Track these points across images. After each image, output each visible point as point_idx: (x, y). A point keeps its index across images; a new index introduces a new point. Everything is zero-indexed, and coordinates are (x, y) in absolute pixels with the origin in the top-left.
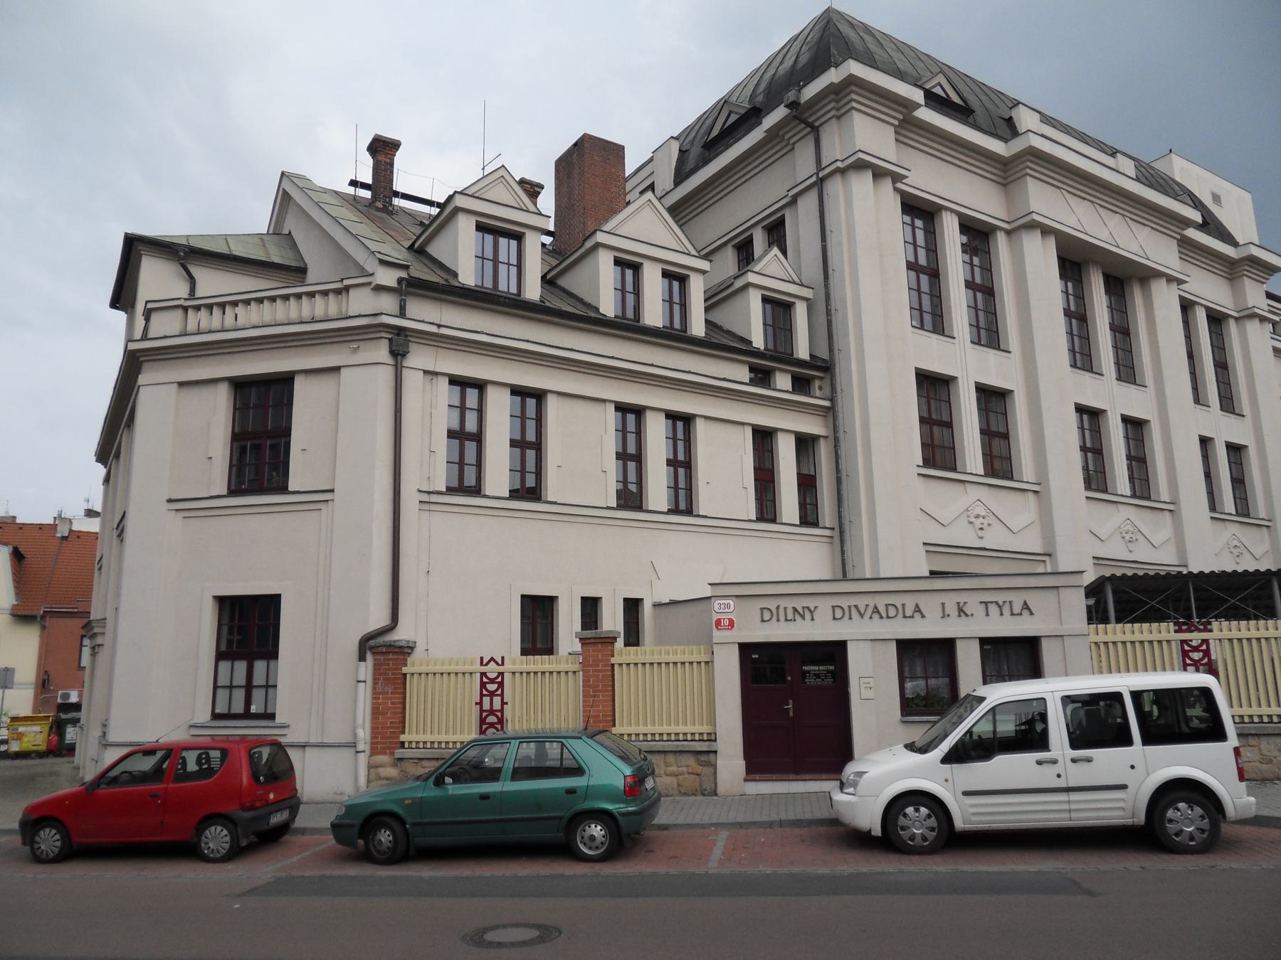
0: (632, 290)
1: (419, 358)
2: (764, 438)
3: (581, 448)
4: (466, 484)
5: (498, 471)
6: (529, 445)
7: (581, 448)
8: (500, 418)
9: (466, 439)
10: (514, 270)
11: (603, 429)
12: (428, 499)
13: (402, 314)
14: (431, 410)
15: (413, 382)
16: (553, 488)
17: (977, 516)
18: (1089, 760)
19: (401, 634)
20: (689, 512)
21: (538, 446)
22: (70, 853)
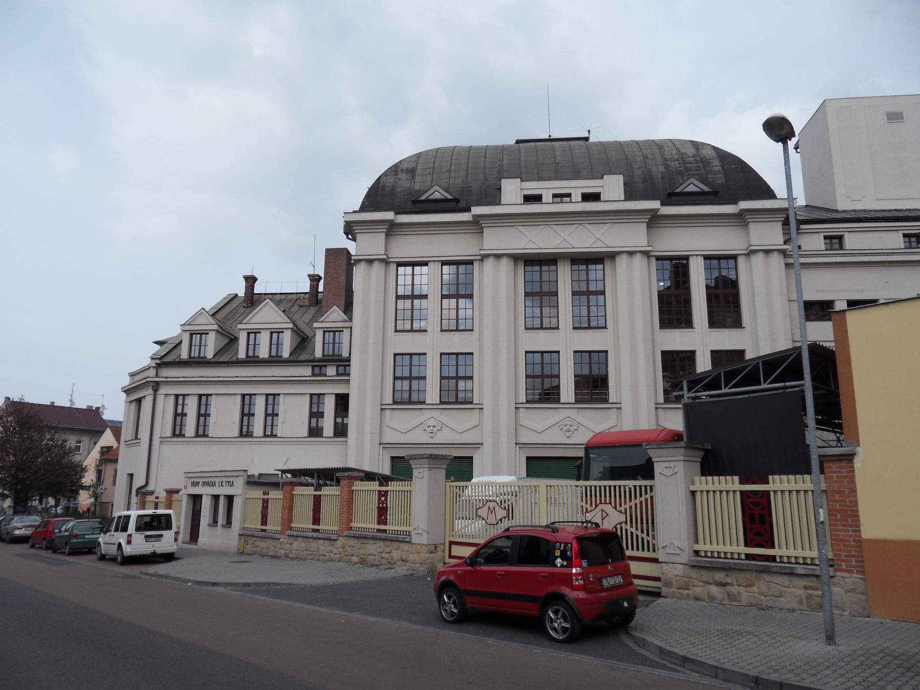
0: (252, 345)
1: (163, 390)
2: (316, 399)
3: (225, 415)
4: (178, 433)
5: (258, 426)
6: (203, 415)
7: (225, 415)
8: (259, 406)
9: (179, 416)
10: (326, 341)
11: (303, 406)
12: (163, 440)
13: (157, 376)
14: (166, 408)
15: (160, 398)
16: (211, 432)
17: (429, 426)
18: (162, 536)
19: (150, 488)
20: (273, 435)
21: (243, 415)
22: (465, 618)
